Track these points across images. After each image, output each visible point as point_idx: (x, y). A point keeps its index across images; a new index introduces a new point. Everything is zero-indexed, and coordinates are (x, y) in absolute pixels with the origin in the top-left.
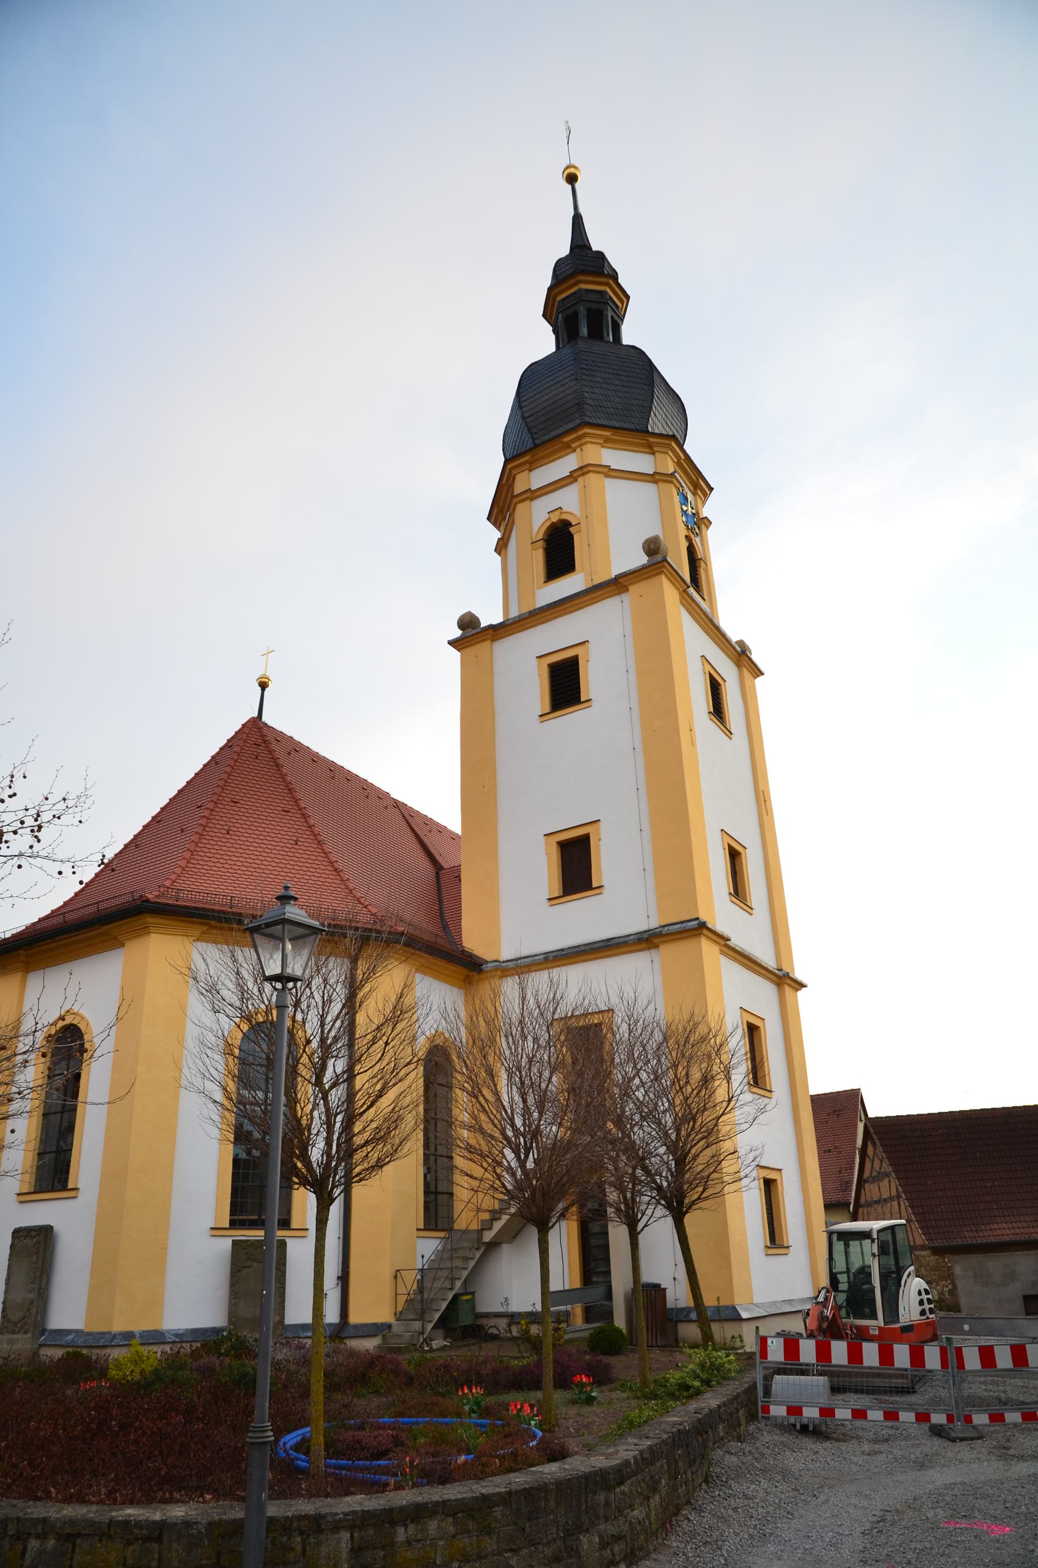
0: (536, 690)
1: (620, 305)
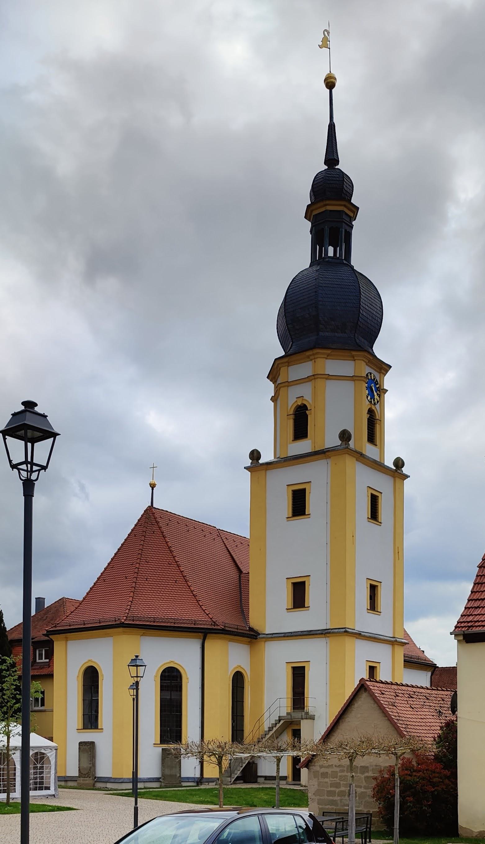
0: (285, 504)
1: (351, 214)
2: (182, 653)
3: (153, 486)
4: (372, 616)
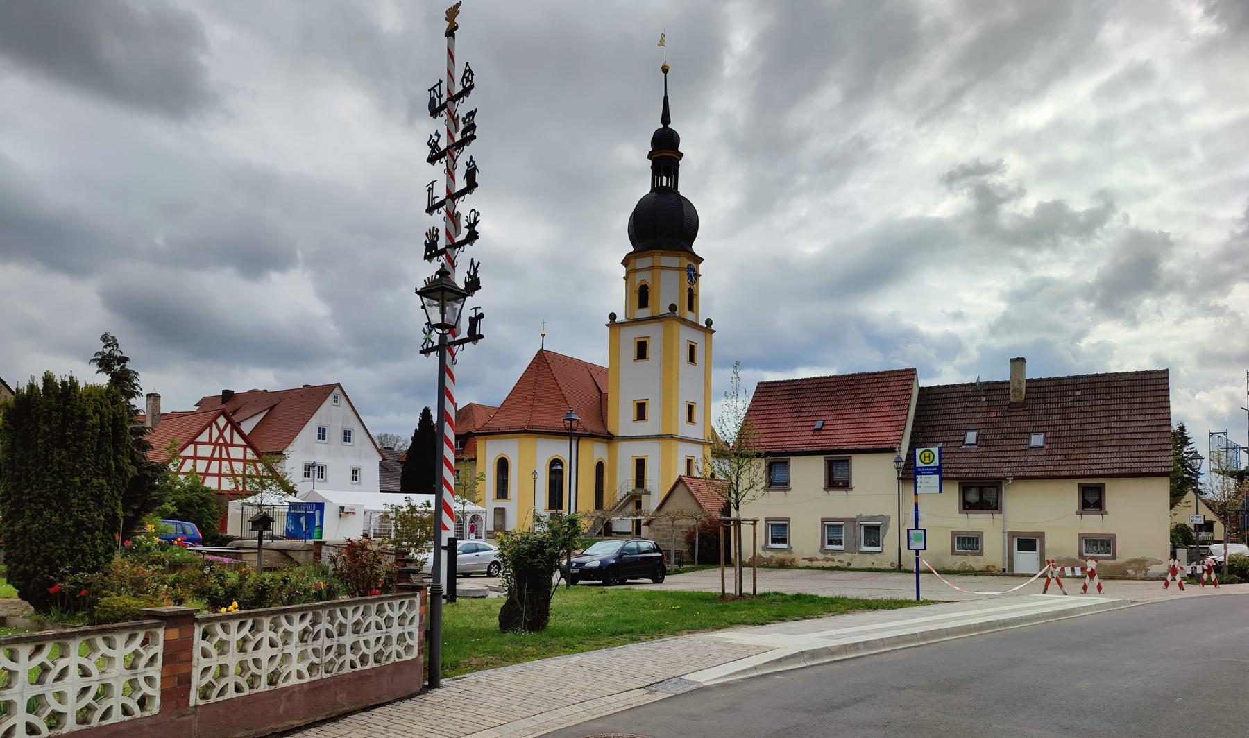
2: (560, 448)
3: (543, 335)
4: (690, 426)
